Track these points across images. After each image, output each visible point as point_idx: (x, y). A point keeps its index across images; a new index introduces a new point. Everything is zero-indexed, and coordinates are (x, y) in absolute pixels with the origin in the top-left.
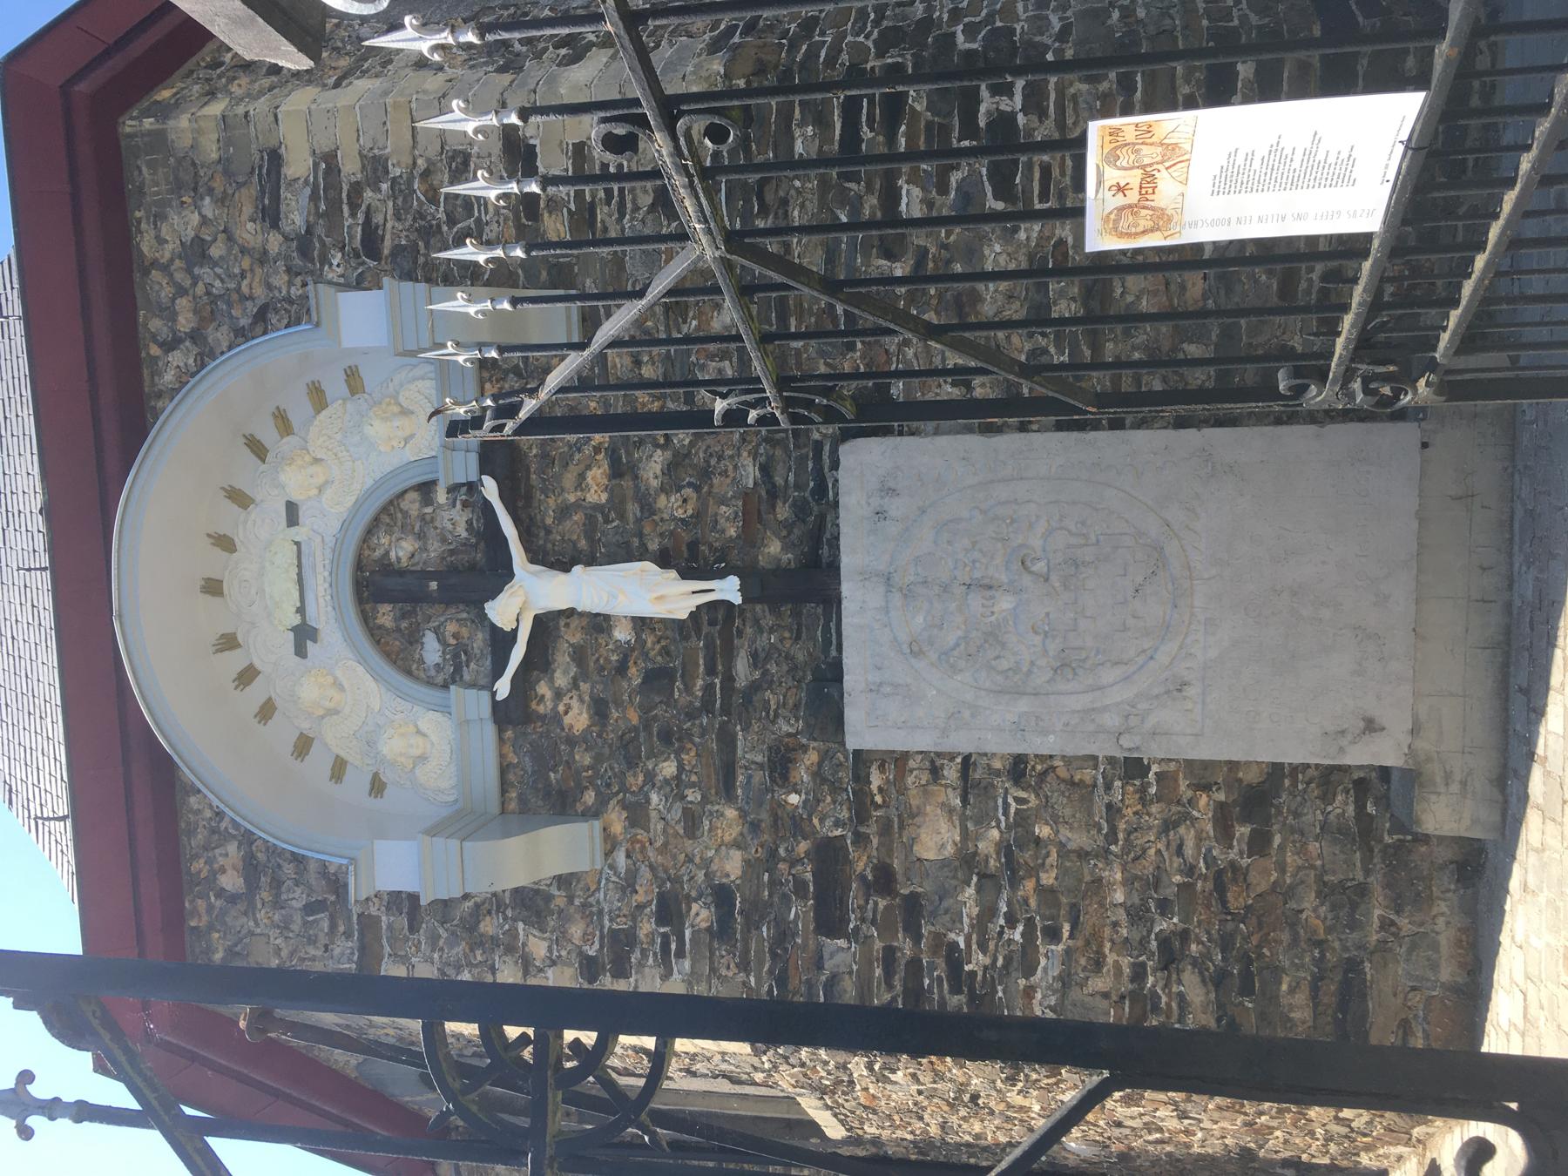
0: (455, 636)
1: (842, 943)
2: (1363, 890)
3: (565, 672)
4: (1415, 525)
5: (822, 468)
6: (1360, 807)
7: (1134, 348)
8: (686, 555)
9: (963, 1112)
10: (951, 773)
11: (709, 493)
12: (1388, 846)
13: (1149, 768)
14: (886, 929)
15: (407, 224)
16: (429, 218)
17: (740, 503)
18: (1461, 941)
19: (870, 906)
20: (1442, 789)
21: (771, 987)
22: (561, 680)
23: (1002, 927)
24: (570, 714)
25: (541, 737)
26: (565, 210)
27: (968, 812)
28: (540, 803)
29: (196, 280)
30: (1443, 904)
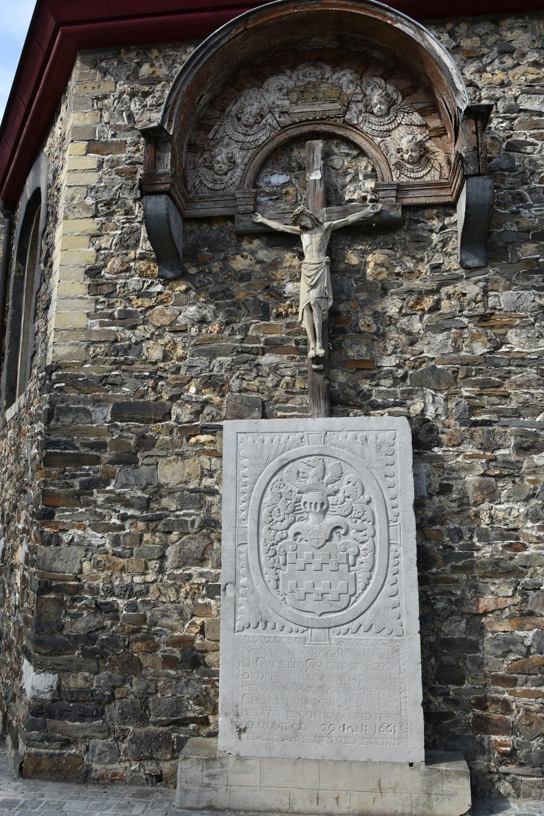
0: (287, 193)
1: (109, 418)
2: (143, 720)
3: (266, 256)
4: (364, 759)
5: (389, 407)
6: (193, 720)
7: (463, 591)
8: (337, 326)
9: (18, 484)
10: (207, 482)
11: (374, 340)
12: (170, 735)
13: (213, 598)
14: (117, 444)
15: (527, 166)
16: (531, 178)
17: (368, 358)
18: (116, 776)
19: (130, 435)
20: (205, 773)
21: (83, 376)
22: (262, 254)
23: (119, 511)
24: (242, 259)
25: (228, 242)
26: (539, 256)
27: (185, 492)
28: (190, 242)
29: (490, 48)
30: (137, 766)
